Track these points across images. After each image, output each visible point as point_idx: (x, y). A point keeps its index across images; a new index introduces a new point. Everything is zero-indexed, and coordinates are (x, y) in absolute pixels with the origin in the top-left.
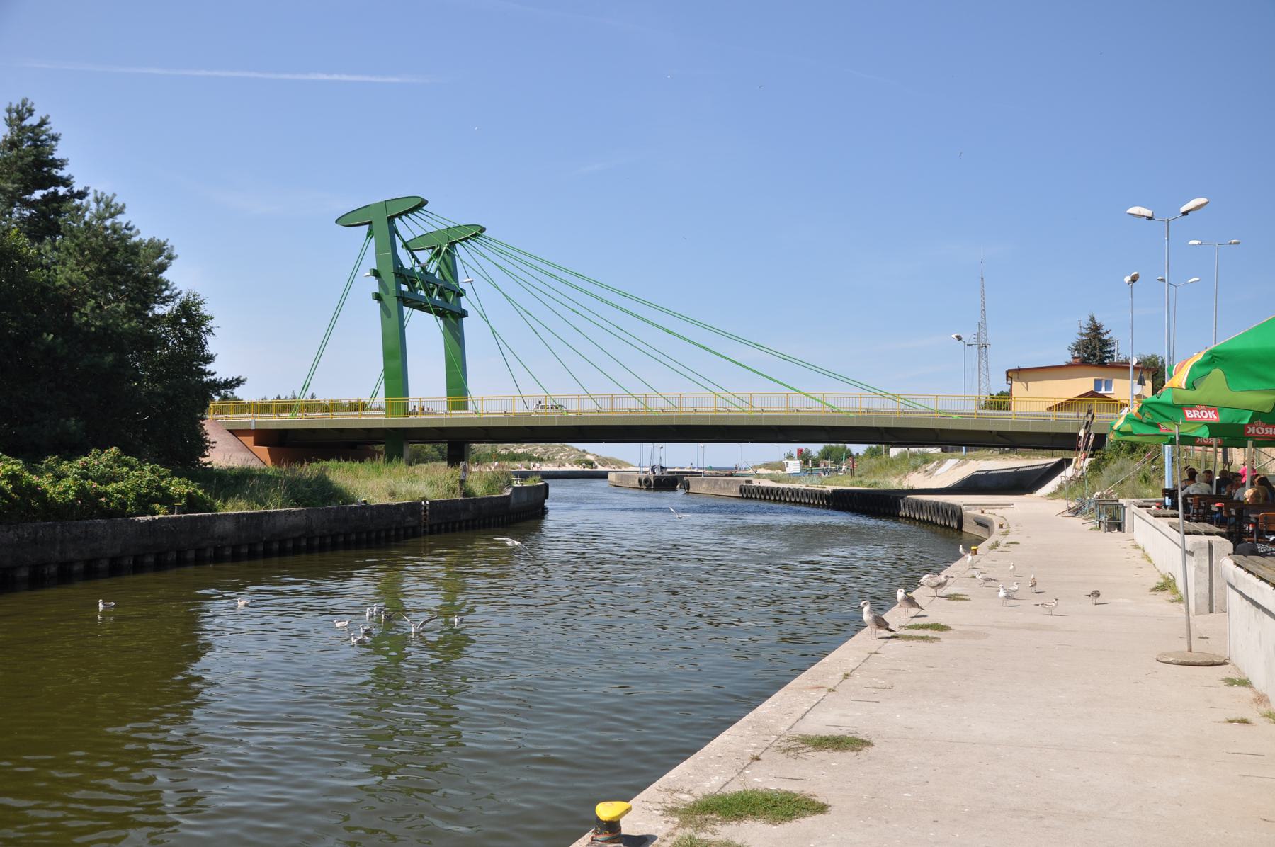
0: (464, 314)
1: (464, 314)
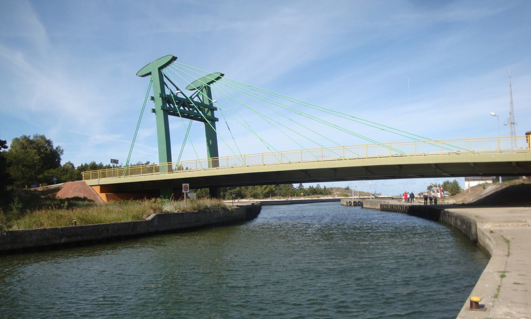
0: (217, 120)
1: (217, 120)
